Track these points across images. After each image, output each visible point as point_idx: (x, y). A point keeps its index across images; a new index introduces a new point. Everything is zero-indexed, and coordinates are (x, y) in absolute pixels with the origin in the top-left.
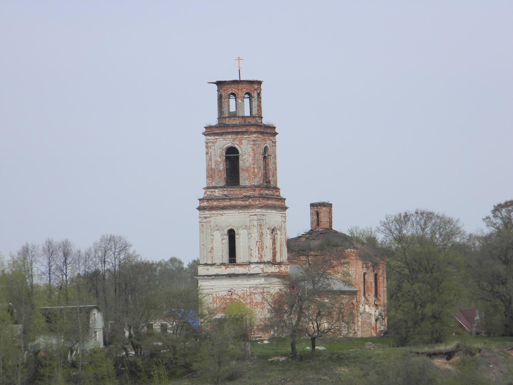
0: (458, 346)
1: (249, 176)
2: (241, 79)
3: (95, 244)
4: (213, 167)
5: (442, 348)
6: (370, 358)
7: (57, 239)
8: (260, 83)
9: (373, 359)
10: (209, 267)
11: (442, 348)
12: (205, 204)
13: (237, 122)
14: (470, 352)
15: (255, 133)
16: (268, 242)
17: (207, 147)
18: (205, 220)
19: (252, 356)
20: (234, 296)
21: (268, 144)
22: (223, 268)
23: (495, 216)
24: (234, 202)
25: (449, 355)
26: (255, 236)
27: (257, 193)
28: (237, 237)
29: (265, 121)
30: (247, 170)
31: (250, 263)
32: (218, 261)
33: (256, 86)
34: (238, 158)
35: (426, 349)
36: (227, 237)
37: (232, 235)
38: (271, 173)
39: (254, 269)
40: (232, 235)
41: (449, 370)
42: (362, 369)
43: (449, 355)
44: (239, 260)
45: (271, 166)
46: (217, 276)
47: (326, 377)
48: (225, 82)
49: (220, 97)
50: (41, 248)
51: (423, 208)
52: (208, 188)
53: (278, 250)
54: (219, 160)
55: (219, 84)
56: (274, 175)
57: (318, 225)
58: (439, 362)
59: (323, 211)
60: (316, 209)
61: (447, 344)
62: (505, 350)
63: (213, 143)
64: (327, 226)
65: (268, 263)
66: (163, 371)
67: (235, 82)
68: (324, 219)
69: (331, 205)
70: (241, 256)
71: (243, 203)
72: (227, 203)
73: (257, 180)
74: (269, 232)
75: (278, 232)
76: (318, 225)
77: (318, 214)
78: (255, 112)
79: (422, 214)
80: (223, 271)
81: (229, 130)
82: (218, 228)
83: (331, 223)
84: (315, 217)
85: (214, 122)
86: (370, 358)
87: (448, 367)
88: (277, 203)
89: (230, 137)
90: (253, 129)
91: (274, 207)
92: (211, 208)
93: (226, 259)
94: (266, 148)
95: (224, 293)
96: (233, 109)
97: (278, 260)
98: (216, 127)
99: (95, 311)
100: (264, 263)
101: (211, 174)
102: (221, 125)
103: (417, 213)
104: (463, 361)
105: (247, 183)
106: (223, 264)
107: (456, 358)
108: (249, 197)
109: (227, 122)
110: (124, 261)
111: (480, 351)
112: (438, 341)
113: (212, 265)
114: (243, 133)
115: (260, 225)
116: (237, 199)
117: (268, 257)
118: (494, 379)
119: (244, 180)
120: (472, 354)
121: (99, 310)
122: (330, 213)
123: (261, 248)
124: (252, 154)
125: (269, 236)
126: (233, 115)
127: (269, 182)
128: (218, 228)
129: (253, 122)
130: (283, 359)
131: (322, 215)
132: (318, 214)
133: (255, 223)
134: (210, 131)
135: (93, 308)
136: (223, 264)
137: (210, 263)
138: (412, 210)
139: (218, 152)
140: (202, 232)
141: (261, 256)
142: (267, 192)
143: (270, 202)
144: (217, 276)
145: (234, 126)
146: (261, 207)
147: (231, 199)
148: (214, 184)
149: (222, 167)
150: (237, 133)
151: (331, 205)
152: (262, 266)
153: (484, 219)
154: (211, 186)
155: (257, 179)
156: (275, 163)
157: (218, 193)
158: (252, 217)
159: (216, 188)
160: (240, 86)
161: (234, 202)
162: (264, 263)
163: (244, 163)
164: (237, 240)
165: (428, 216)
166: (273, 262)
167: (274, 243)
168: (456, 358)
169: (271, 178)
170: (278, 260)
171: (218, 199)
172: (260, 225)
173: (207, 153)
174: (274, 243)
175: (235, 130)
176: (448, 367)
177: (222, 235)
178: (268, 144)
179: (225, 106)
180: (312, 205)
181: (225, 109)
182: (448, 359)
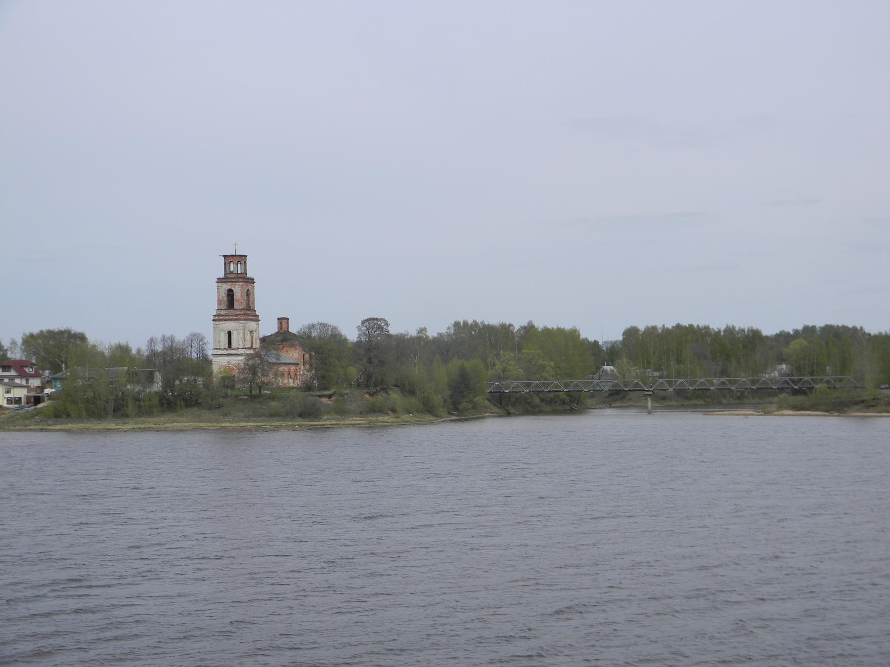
0: (335, 392)
1: (239, 304)
2: (237, 254)
3: (187, 337)
4: (221, 299)
5: (327, 392)
6: (289, 397)
7: (168, 334)
8: (246, 256)
9: (290, 398)
10: (218, 350)
11: (327, 392)
12: (216, 318)
13: (233, 276)
14: (342, 395)
15: (242, 282)
16: (248, 337)
17: (218, 289)
18: (216, 326)
19: (231, 396)
20: (230, 365)
21: (250, 287)
22: (225, 350)
23: (363, 326)
24: (231, 317)
25: (330, 396)
26: (241, 334)
27: (242, 313)
28: (232, 335)
29: (248, 276)
30: (238, 301)
31: (239, 348)
32: (223, 347)
33: (243, 258)
34: (233, 294)
35: (318, 393)
36: (227, 335)
37: (230, 333)
38: (251, 302)
39: (241, 351)
40: (230, 333)
41: (329, 404)
42: (283, 403)
43: (330, 396)
44: (233, 347)
45: (251, 299)
46: (222, 355)
47: (265, 407)
48: (227, 255)
49: (225, 264)
50: (160, 338)
51: (321, 321)
52: (218, 310)
53: (254, 341)
54: (224, 295)
55: (224, 256)
56: (253, 303)
57: (281, 329)
58: (324, 400)
59: (284, 322)
60: (280, 321)
61: (331, 390)
62: (362, 394)
63: (221, 287)
64: (286, 330)
65: (248, 348)
66: (183, 403)
67: (232, 256)
68: (284, 326)
69: (288, 319)
70: (233, 346)
71: (235, 318)
72: (227, 318)
73: (242, 306)
74: (249, 332)
75: (255, 333)
76: (281, 329)
77: (281, 323)
78: (243, 271)
79: (321, 324)
80: (225, 352)
81: (229, 280)
82: (223, 330)
83: (288, 328)
84: (280, 325)
85: (222, 275)
86: (289, 397)
87: (329, 402)
88: (254, 318)
89: (229, 284)
90: (241, 280)
91: (252, 320)
92: (219, 320)
93: (227, 346)
94: (248, 289)
95: (226, 363)
96: (232, 269)
97: (254, 347)
98: (222, 278)
99: (157, 372)
100: (246, 348)
101: (220, 302)
102: (225, 278)
103: (318, 324)
104: (337, 400)
105: (238, 308)
106: (225, 349)
107: (333, 398)
108: (238, 315)
109: (229, 276)
110: (705, 330)
111: (347, 394)
112: (326, 389)
113: (219, 349)
114: (236, 282)
115: (244, 329)
116: (232, 316)
117: (248, 345)
118: (354, 409)
119: (237, 306)
120: (342, 396)
121: (159, 372)
122: (288, 322)
123: (244, 341)
124: (240, 293)
125: (249, 335)
126: (232, 273)
127: (250, 307)
128: (223, 330)
129: (241, 276)
130: (246, 397)
131: (283, 324)
132: (281, 323)
133: (241, 328)
134: (220, 281)
135: (156, 371)
136: (225, 349)
137: (218, 348)
138: (315, 322)
139: (223, 292)
140: (214, 332)
141: (244, 345)
142: (248, 312)
143: (250, 317)
144: (222, 355)
145: (232, 278)
146: (244, 320)
147: (229, 316)
148: (221, 308)
149: (225, 299)
150: (233, 282)
151: (288, 319)
152: (244, 350)
153: (357, 327)
154: (220, 308)
155: (242, 306)
156: (254, 297)
157: (223, 312)
158: (240, 325)
159: (222, 310)
160: (235, 258)
161: (231, 317)
162: (246, 348)
163: (236, 297)
164: (232, 336)
165: (324, 325)
166: (252, 348)
167: (252, 338)
168: (333, 398)
169: (251, 305)
170: (254, 347)
171: (223, 316)
172: (244, 329)
173: (218, 292)
174: (252, 338)
175: (232, 280)
176: (329, 402)
177: (225, 334)
178: (250, 287)
179: (228, 267)
180: (278, 319)
181: (228, 270)
182: (329, 398)
